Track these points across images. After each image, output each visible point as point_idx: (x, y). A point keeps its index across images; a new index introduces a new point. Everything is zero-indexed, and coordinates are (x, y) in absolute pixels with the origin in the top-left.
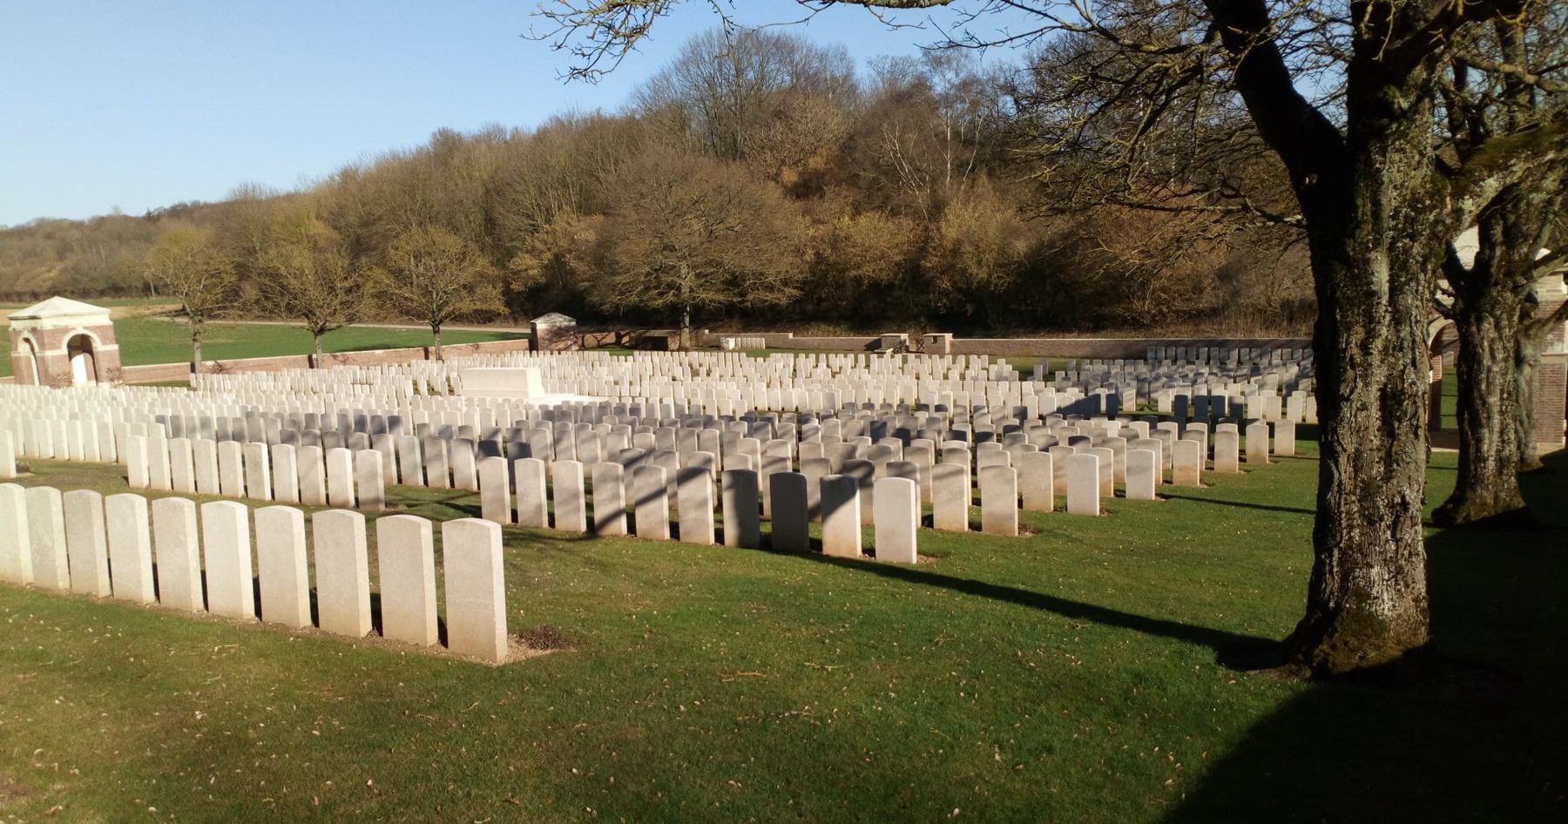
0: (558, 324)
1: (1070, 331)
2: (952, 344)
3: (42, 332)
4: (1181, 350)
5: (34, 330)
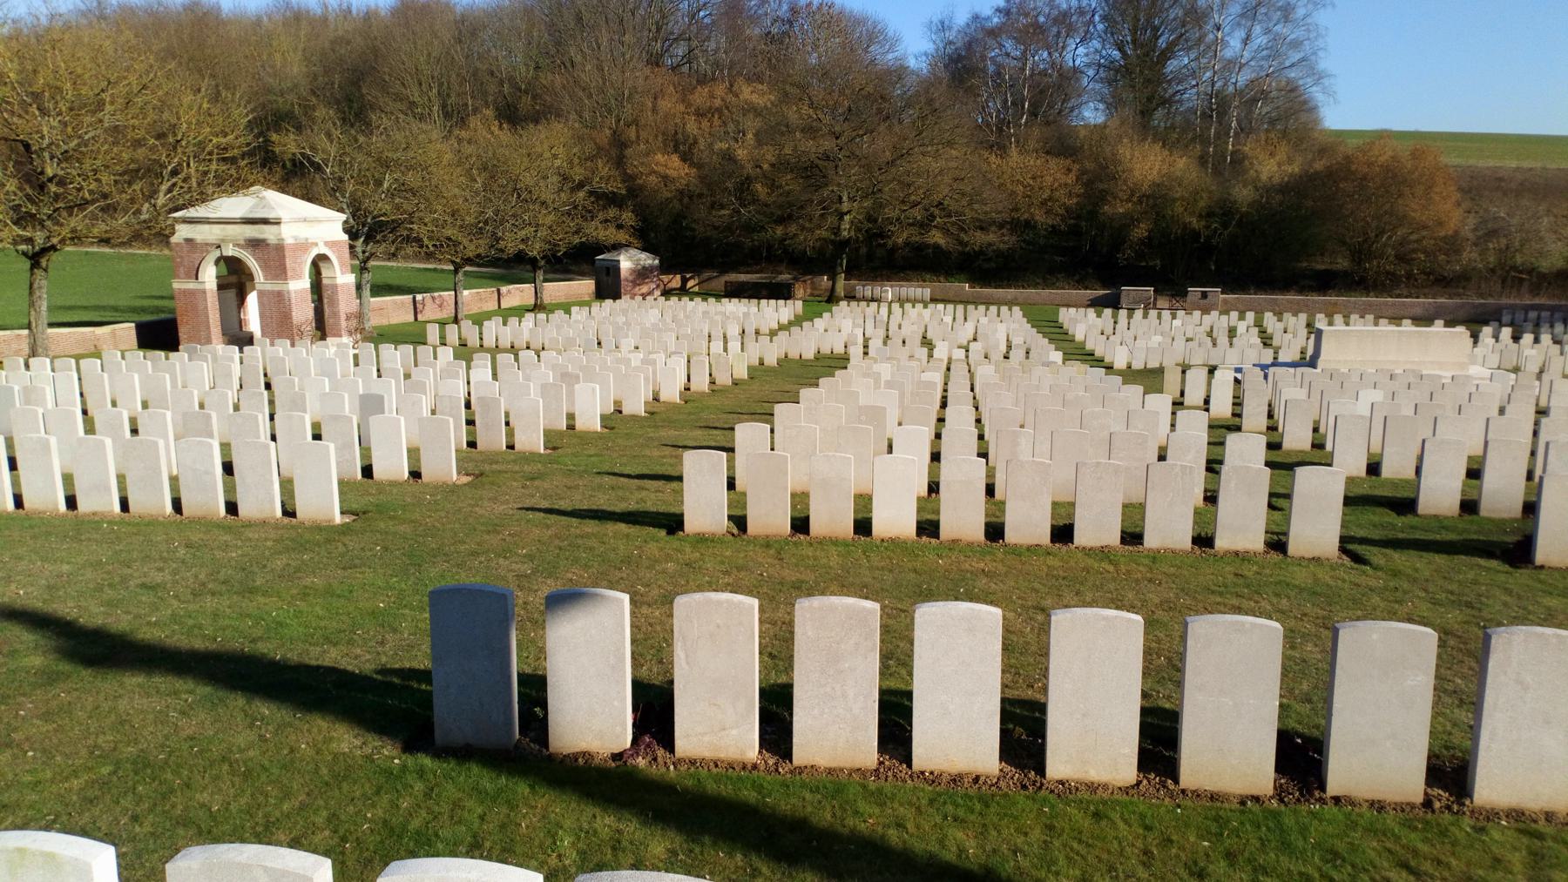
1: (1288, 291)
3: (280, 248)
5: (255, 244)
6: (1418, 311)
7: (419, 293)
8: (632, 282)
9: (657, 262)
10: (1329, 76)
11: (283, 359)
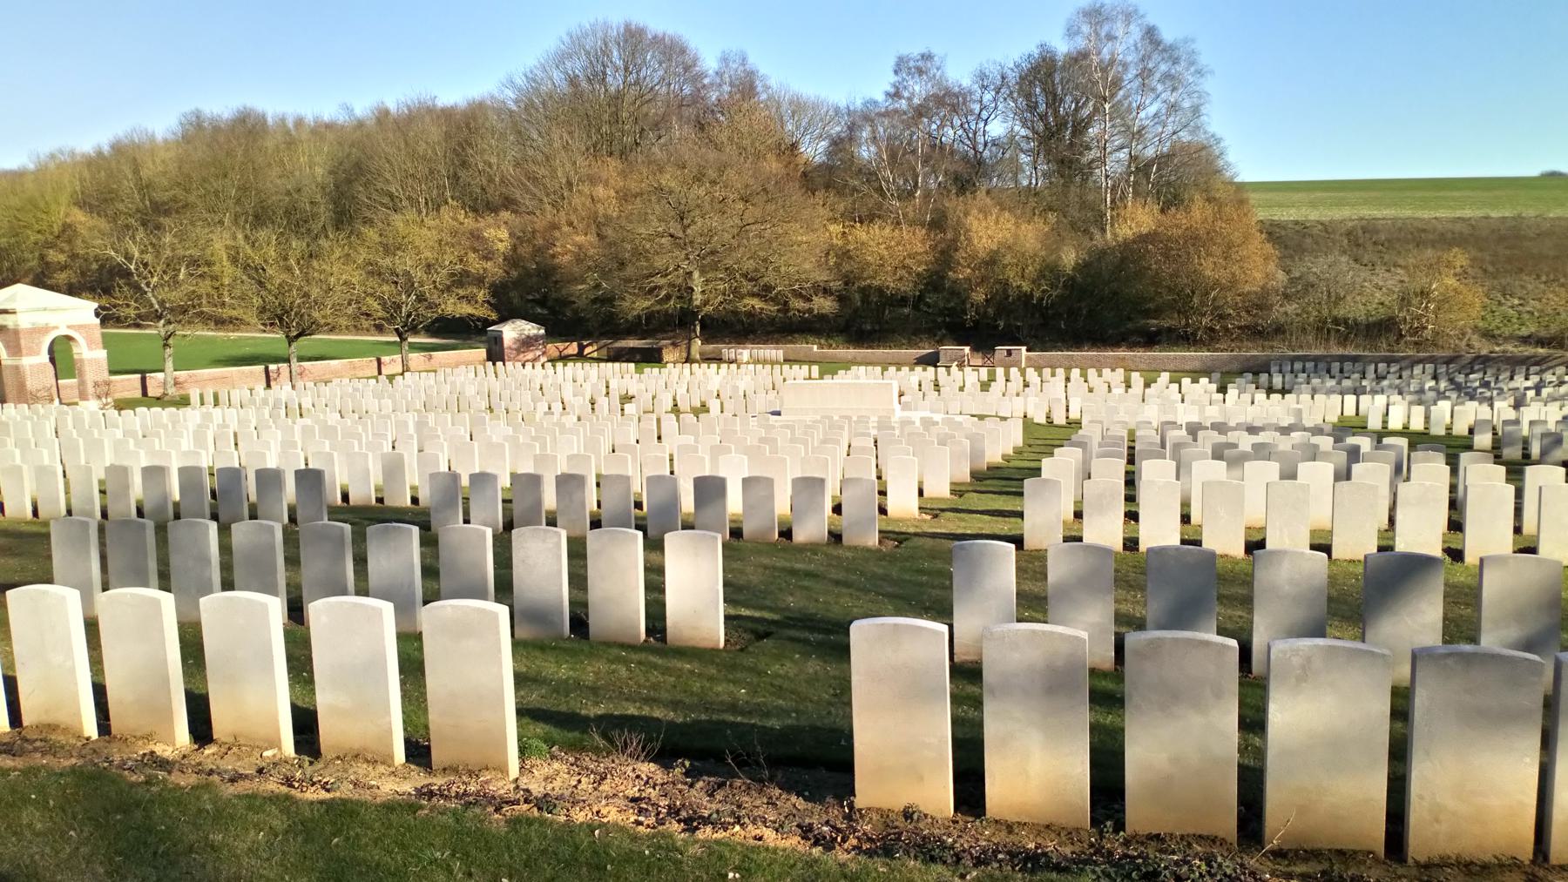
0: (526, 333)
2: (1028, 358)
3: (16, 332)
4: (1310, 365)
6: (1197, 365)
7: (272, 362)
8: (516, 350)
9: (542, 331)
10: (38, 157)
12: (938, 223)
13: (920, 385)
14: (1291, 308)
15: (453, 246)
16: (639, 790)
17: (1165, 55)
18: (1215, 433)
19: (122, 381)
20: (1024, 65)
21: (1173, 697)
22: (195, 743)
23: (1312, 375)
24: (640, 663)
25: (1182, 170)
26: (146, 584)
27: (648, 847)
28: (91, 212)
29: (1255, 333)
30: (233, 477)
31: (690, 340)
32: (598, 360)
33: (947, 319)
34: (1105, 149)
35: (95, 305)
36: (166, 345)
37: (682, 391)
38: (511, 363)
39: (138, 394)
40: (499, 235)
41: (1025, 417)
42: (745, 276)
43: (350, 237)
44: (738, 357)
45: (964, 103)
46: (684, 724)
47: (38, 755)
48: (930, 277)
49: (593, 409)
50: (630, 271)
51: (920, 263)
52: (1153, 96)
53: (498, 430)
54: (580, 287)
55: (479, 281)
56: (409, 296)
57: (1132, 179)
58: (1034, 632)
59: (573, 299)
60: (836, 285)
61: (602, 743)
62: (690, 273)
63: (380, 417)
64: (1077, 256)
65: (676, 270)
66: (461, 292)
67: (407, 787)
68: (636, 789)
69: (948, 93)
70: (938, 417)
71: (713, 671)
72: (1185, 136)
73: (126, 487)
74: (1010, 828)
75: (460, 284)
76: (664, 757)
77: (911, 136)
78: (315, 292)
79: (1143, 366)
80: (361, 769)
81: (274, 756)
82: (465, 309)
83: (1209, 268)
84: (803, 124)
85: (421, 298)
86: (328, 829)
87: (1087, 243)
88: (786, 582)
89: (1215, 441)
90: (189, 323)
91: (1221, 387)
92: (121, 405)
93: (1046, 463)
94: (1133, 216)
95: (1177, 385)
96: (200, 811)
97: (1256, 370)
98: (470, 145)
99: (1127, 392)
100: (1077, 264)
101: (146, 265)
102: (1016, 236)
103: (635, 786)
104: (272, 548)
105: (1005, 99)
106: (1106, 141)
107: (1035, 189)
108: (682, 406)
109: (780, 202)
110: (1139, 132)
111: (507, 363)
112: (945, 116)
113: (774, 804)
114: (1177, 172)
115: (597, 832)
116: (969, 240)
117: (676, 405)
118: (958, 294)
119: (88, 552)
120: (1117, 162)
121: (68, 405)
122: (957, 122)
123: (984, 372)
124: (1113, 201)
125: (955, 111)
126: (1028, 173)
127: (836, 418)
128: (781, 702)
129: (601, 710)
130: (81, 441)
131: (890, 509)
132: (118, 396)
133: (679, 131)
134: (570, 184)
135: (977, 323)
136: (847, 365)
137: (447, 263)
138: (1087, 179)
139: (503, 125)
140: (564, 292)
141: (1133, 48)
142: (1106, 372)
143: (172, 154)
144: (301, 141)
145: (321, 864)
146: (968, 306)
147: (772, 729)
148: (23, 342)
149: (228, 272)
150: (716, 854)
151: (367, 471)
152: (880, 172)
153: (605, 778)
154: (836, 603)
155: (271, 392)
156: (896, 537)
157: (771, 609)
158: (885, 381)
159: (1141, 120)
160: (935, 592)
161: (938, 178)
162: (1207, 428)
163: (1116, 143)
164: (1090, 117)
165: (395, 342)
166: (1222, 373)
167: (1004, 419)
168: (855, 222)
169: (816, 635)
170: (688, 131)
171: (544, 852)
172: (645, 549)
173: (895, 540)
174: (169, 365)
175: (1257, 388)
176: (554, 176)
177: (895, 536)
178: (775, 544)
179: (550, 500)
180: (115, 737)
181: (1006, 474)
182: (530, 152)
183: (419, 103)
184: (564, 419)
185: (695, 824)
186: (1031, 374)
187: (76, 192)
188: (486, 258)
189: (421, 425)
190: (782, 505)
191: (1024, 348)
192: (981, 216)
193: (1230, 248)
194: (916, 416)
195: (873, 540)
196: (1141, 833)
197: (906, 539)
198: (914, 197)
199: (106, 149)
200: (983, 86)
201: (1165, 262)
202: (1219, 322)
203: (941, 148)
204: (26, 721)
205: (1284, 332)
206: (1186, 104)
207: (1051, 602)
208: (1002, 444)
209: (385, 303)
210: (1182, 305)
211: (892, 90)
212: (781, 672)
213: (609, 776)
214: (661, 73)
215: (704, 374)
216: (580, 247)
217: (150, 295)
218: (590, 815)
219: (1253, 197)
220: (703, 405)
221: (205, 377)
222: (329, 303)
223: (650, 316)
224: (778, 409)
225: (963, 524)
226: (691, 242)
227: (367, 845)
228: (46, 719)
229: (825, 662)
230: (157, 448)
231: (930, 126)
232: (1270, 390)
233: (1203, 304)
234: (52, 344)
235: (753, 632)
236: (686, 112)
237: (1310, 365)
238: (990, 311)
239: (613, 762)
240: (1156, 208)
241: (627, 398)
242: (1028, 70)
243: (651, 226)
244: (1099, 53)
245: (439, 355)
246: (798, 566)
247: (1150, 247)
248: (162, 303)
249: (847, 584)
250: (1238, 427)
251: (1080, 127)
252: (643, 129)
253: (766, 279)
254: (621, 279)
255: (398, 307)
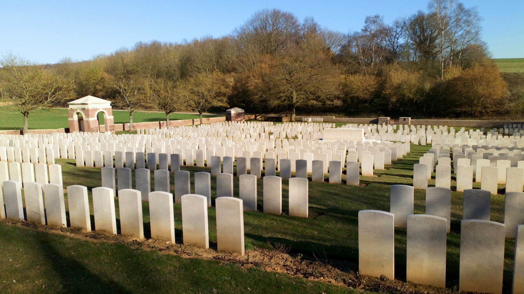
0: (238, 112)
2: (411, 122)
3: (88, 110)
5: (83, 109)
6: (475, 125)
9: (243, 111)
10: (94, 57)
11: (92, 144)
12: (379, 74)
13: (371, 131)
14: (512, 105)
15: (217, 84)
16: (284, 263)
17: (466, 14)
18: (483, 150)
19: (118, 126)
20: (412, 18)
21: (480, 243)
22: (145, 238)
23: (520, 129)
24: (280, 221)
25: (471, 54)
26: (128, 188)
27: (294, 282)
28: (109, 74)
29: (498, 113)
30: (152, 156)
31: (292, 114)
32: (261, 121)
33: (382, 108)
34: (442, 47)
35: (110, 102)
36: (131, 115)
37: (289, 131)
38: (233, 121)
39: (122, 130)
40: (231, 80)
41: (410, 142)
42: (311, 93)
43: (185, 81)
44: (308, 120)
45: (390, 32)
46: (297, 242)
47: (103, 239)
48: (376, 93)
49: (260, 137)
50: (272, 91)
51: (372, 88)
52: (460, 28)
53: (230, 143)
54: (256, 97)
55: (224, 95)
56: (203, 100)
57: (452, 58)
58: (427, 218)
59: (254, 101)
60: (342, 96)
61: (271, 246)
62: (292, 92)
63: (194, 138)
64: (431, 86)
65: (287, 91)
66: (219, 99)
67: (210, 256)
68: (283, 262)
69: (385, 29)
70: (379, 142)
71: (305, 225)
72: (472, 43)
73: (121, 158)
74: (415, 286)
75: (218, 96)
76: (293, 253)
77: (370, 44)
78: (175, 98)
79: (454, 125)
80: (196, 249)
81: (169, 243)
82: (220, 104)
83: (481, 90)
84: (332, 41)
85: (206, 101)
86: (192, 267)
87: (434, 81)
88: (328, 196)
89: (484, 152)
90: (138, 108)
91: (485, 133)
92: (117, 133)
93: (421, 159)
94: (452, 71)
95: (468, 132)
96: (153, 259)
97: (498, 127)
98: (223, 51)
99: (448, 134)
100: (431, 88)
101: (125, 90)
102: (408, 79)
103: (282, 261)
104: (166, 178)
105: (405, 31)
106: (442, 45)
107: (415, 62)
108: (289, 136)
109: (324, 68)
110: (455, 41)
111: (232, 122)
112: (383, 37)
113: (330, 271)
114: (469, 55)
115: (277, 275)
116: (391, 80)
117: (287, 136)
118: (386, 99)
119: (112, 177)
120: (446, 52)
121: (102, 133)
122: (387, 39)
123: (395, 126)
124: (444, 66)
125: (387, 35)
126: (413, 56)
127: (342, 141)
128: (329, 237)
129: (269, 235)
130: (107, 144)
131: (363, 173)
132: (116, 130)
133: (290, 45)
134: (254, 63)
135: (392, 109)
136: (345, 123)
137: (215, 89)
138: (435, 58)
139: (233, 45)
140: (251, 98)
141: (453, 11)
142: (441, 127)
143: (133, 55)
144: (171, 51)
145: (191, 278)
146: (390, 103)
147: (327, 246)
148: (90, 113)
149: (149, 92)
150: (317, 285)
151: (192, 155)
152: (359, 57)
153: (272, 258)
154: (346, 204)
155: (161, 130)
156: (365, 183)
157: (323, 205)
158: (359, 129)
159: (456, 37)
160: (381, 202)
161: (380, 58)
162: (480, 148)
163: (446, 45)
164: (436, 36)
165: (198, 115)
166: (485, 128)
167: (403, 143)
168: (350, 74)
169: (339, 215)
170: (293, 45)
171: (260, 280)
172: (154, 191)
173: (365, 184)
174: (131, 121)
175: (499, 134)
176: (249, 60)
177: (365, 182)
178: (323, 183)
179: (248, 166)
180: (122, 235)
181: (404, 162)
182: (241, 53)
183: (207, 38)
184: (251, 140)
185: (307, 275)
186: (413, 127)
187: (105, 67)
188: (227, 88)
189: (207, 141)
190: (325, 171)
191: (410, 118)
192: (395, 71)
193: (489, 83)
194: (371, 141)
195: (357, 183)
196: (465, 291)
197: (369, 184)
198: (371, 65)
199: (114, 54)
200: (397, 26)
201: (464, 88)
202: (484, 109)
203: (381, 48)
204: (96, 229)
205: (509, 113)
206: (473, 31)
207: (427, 208)
208: (403, 151)
209: (195, 102)
210: (470, 103)
211: (364, 29)
212: (328, 227)
213: (273, 257)
214: (285, 25)
215: (296, 126)
216: (256, 84)
217: (126, 99)
218: (271, 270)
219: (498, 64)
220: (296, 136)
221: (142, 125)
222: (179, 102)
223: (279, 106)
224: (321, 138)
225: (390, 179)
226: (293, 82)
227: (204, 273)
228: (102, 228)
229: (344, 224)
230: (129, 147)
231: (377, 40)
232: (504, 135)
233: (478, 103)
234: (98, 113)
235: (318, 212)
236: (292, 38)
237: (519, 125)
238: (398, 105)
239: (274, 253)
240: (461, 68)
241: (271, 133)
242: (414, 20)
243: (280, 77)
244: (440, 14)
245: (211, 119)
246: (332, 191)
247: (458, 82)
248: (130, 102)
249: (348, 198)
250: (492, 147)
251: (433, 40)
252: (278, 45)
253: (318, 94)
254: (269, 94)
255: (199, 103)
